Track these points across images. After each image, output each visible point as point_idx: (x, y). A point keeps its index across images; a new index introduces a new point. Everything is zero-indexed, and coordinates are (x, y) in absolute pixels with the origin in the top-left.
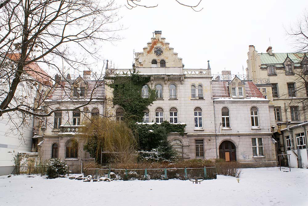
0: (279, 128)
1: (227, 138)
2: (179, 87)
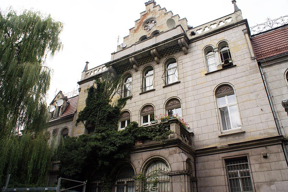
2: (181, 61)
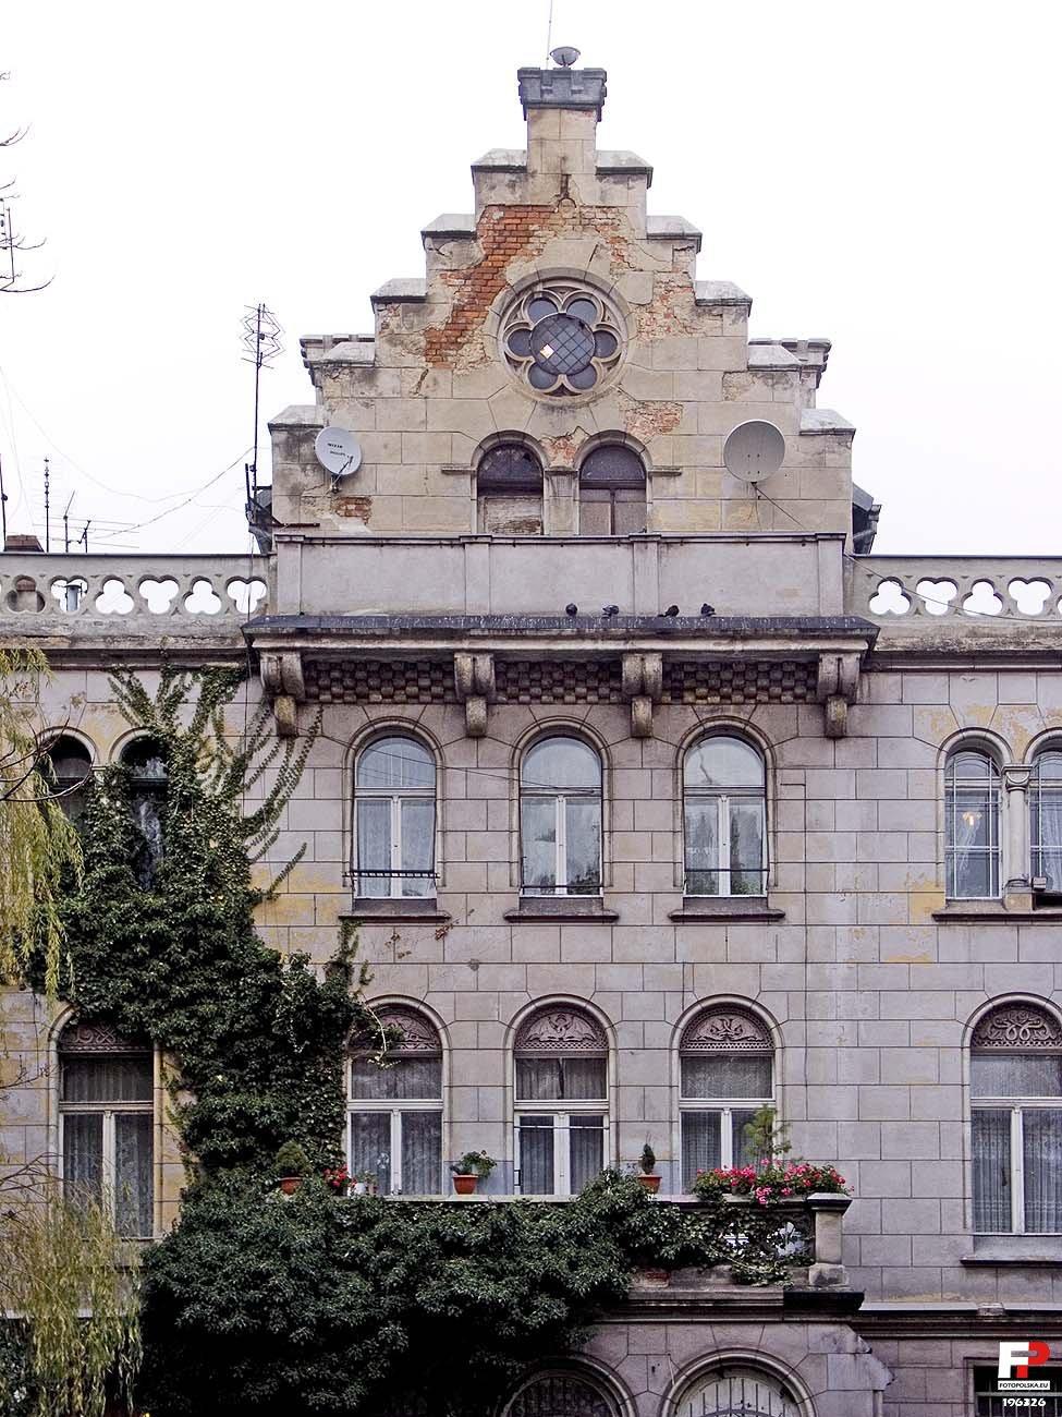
2: (797, 776)
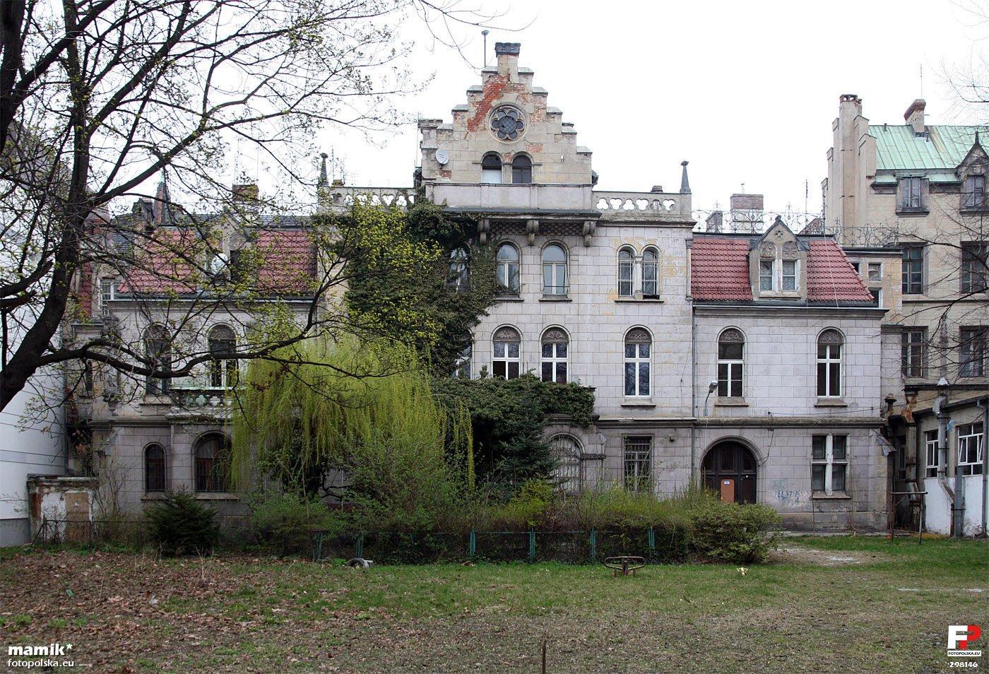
0: (908, 402)
1: (734, 433)
2: (576, 258)
